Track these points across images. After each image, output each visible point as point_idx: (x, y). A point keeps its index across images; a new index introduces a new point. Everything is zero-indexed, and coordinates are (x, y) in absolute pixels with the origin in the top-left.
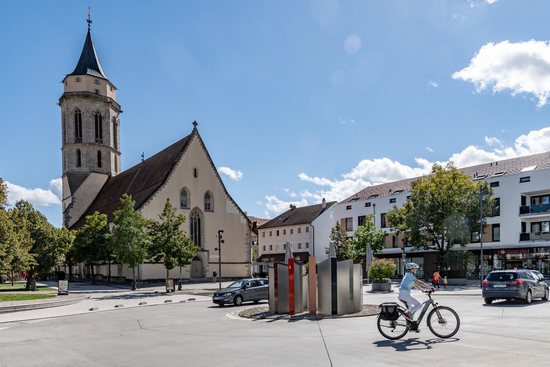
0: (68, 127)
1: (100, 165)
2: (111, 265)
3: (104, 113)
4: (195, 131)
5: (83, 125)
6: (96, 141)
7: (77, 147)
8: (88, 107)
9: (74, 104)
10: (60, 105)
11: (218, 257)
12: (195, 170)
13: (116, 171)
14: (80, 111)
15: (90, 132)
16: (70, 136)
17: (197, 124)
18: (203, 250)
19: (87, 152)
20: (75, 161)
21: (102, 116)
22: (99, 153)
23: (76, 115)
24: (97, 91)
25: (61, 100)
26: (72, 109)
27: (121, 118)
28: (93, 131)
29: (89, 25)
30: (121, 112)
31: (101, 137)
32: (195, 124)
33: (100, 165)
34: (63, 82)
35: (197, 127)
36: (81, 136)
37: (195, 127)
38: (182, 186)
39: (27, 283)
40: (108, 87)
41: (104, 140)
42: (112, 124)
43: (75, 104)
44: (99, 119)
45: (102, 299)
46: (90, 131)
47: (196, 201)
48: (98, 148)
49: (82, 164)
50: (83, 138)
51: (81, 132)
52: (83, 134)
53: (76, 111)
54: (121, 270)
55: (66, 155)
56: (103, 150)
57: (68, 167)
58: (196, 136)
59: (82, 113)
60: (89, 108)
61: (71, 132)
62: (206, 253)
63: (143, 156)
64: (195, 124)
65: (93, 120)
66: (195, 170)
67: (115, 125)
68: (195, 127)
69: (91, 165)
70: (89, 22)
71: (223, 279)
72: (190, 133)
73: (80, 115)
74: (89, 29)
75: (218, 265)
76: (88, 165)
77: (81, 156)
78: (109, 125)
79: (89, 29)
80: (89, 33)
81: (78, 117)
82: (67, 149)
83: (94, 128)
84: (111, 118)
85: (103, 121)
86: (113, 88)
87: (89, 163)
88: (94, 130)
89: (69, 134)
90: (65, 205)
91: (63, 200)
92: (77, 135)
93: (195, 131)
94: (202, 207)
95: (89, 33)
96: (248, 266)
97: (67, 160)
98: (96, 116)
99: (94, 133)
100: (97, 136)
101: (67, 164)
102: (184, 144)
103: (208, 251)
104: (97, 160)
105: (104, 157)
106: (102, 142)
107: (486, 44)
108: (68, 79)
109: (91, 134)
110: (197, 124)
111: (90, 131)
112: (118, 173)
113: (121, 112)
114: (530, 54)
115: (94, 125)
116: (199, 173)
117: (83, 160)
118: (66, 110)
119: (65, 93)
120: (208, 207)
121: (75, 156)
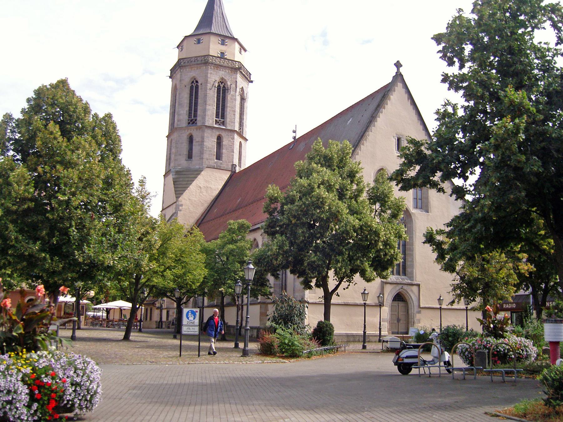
0: (179, 105)
1: (219, 156)
2: (205, 309)
4: (399, 77)
6: (217, 122)
7: (189, 132)
9: (188, 75)
10: (170, 77)
11: (201, 344)
13: (240, 166)
14: (197, 82)
16: (181, 117)
17: (401, 66)
20: (185, 152)
21: (226, 86)
22: (219, 138)
23: (192, 88)
24: (222, 53)
25: (173, 71)
26: (187, 80)
27: (251, 90)
30: (252, 82)
31: (223, 116)
32: (398, 65)
33: (219, 156)
34: (178, 47)
35: (401, 70)
36: (195, 116)
37: (398, 69)
38: (377, 168)
40: (237, 46)
41: (228, 120)
42: (238, 98)
43: (191, 74)
44: (222, 91)
49: (194, 155)
51: (196, 111)
53: (193, 82)
55: (174, 145)
56: (223, 134)
57: (175, 160)
58: (400, 85)
59: (199, 84)
61: (183, 112)
62: (415, 288)
63: (294, 132)
64: (398, 65)
67: (243, 99)
68: (398, 69)
72: (389, 80)
73: (197, 87)
78: (235, 100)
81: (195, 89)
82: (175, 136)
84: (238, 90)
86: (243, 48)
89: (179, 115)
90: (165, 216)
91: (163, 210)
93: (399, 77)
97: (173, 150)
100: (217, 116)
101: (173, 156)
102: (381, 96)
103: (418, 285)
105: (225, 145)
106: (223, 123)
107: (476, 181)
108: (185, 43)
110: (401, 66)
112: (242, 168)
113: (252, 82)
118: (178, 83)
119: (179, 60)
121: (185, 144)
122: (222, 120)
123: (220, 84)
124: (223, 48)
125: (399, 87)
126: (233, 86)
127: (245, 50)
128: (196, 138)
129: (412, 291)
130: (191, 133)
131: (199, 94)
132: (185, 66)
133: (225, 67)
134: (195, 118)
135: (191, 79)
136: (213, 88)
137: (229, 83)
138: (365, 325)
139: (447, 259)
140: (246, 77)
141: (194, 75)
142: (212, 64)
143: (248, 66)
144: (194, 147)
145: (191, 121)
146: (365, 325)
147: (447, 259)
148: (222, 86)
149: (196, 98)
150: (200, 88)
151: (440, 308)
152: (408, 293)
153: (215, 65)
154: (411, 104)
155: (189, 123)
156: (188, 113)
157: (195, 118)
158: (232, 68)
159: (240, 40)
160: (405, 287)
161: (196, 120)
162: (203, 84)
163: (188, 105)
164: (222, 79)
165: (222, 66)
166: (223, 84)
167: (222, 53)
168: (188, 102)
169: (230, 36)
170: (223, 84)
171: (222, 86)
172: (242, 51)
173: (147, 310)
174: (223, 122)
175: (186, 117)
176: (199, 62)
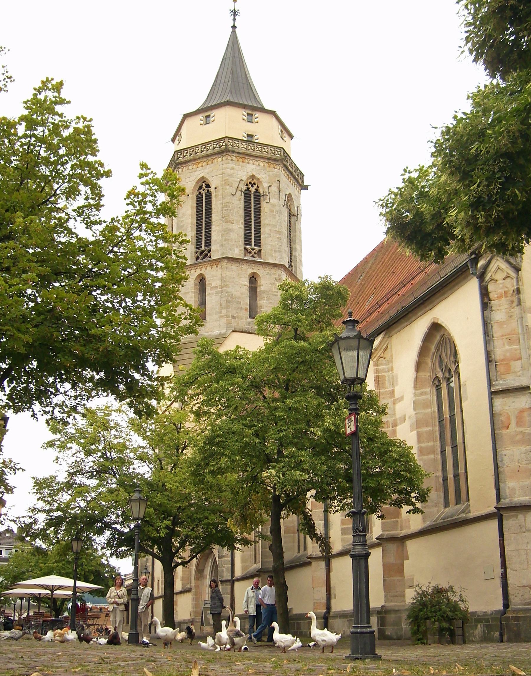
3: (266, 185)
7: (198, 272)
8: (229, 171)
14: (208, 186)
15: (231, 230)
19: (222, 279)
21: (261, 191)
22: (253, 279)
28: (238, 228)
30: (306, 188)
31: (258, 243)
36: (208, 243)
39: (219, 544)
44: (253, 199)
46: (231, 226)
48: (249, 270)
50: (213, 248)
52: (215, 236)
53: (201, 187)
54: (400, 570)
59: (212, 189)
60: (231, 175)
65: (239, 203)
67: (293, 216)
69: (233, 312)
70: (235, 13)
71: (47, 600)
73: (209, 196)
74: (234, 27)
76: (224, 312)
77: (208, 291)
79: (234, 27)
80: (234, 33)
83: (242, 220)
87: (227, 307)
88: (243, 226)
95: (234, 33)
98: (247, 195)
99: (242, 233)
100: (247, 241)
104: (247, 300)
105: (264, 292)
109: (233, 236)
111: (231, 226)
113: (306, 188)
114: (331, 545)
115: (242, 212)
122: (258, 248)
123: (250, 186)
126: (274, 189)
127: (291, 137)
130: (201, 275)
131: (213, 206)
132: (186, 162)
133: (257, 157)
134: (208, 248)
135: (197, 182)
136: (239, 193)
137: (266, 185)
139: (114, 562)
140: (295, 178)
141: (201, 175)
142: (233, 152)
143: (298, 157)
145: (201, 253)
147: (114, 562)
148: (253, 190)
149: (209, 225)
150: (213, 195)
153: (238, 153)
155: (198, 258)
157: (208, 248)
158: (269, 159)
159: (279, 114)
161: (209, 251)
162: (220, 188)
163: (195, 228)
164: (253, 177)
165: (251, 156)
166: (255, 187)
168: (195, 221)
169: (259, 106)
170: (255, 187)
171: (253, 190)
172: (286, 135)
173: (305, 548)
174: (260, 251)
176: (210, 152)
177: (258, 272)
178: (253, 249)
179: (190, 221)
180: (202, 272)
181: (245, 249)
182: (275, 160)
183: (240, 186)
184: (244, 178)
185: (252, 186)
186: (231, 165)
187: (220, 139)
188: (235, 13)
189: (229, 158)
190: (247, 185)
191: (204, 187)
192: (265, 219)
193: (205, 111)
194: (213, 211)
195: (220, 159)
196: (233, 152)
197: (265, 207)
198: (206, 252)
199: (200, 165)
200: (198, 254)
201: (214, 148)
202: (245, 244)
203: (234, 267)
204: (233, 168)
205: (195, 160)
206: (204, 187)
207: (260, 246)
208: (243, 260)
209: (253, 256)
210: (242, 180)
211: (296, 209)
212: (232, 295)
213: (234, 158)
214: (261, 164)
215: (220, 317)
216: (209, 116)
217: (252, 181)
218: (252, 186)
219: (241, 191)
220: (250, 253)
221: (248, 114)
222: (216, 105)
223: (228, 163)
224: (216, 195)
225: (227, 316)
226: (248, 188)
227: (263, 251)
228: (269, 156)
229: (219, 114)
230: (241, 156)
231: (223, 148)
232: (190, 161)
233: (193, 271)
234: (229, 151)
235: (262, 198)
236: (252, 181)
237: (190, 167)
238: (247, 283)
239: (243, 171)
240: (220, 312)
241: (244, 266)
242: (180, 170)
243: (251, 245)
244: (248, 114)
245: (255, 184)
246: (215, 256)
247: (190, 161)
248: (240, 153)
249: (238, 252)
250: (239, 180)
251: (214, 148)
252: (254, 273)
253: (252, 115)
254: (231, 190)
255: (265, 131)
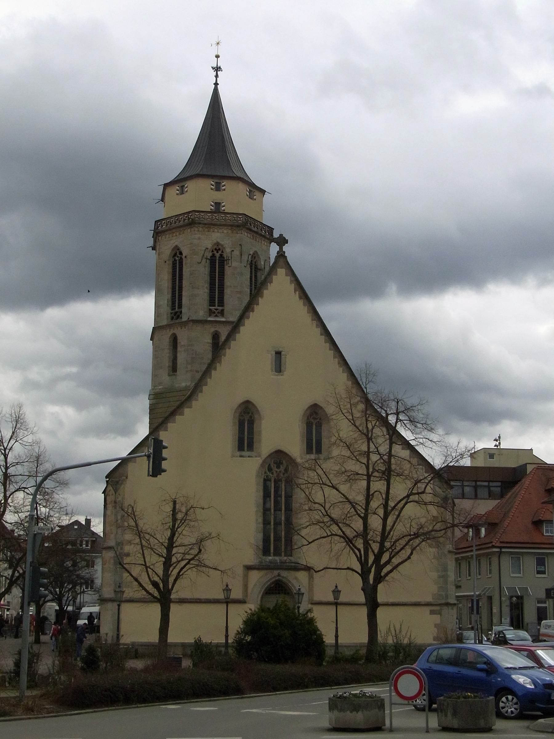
5: (185, 283)
6: (211, 313)
7: (172, 331)
9: (168, 244)
10: (154, 248)
12: (278, 354)
14: (181, 253)
17: (286, 242)
18: (296, 568)
21: (225, 255)
28: (203, 292)
29: (217, 76)
31: (221, 303)
35: (285, 248)
36: (180, 306)
38: (240, 399)
43: (172, 242)
45: (290, 693)
47: (281, 432)
49: (178, 367)
52: (185, 301)
53: (175, 255)
59: (183, 257)
62: (302, 576)
65: (203, 270)
66: (278, 354)
70: (217, 69)
74: (216, 84)
75: (125, 607)
77: (179, 349)
79: (216, 84)
83: (207, 285)
85: (226, 267)
88: (207, 291)
92: (173, 308)
94: (295, 448)
96: (440, 613)
98: (212, 260)
100: (212, 302)
106: (222, 313)
110: (286, 242)
116: (288, 361)
117: (181, 357)
120: (314, 444)
121: (167, 351)
122: (220, 308)
123: (215, 252)
124: (218, 196)
125: (281, 272)
126: (237, 253)
127: (263, 192)
128: (182, 341)
129: (296, 578)
133: (220, 225)
134: (180, 310)
135: (173, 250)
136: (204, 260)
137: (228, 250)
138: (337, 628)
141: (176, 244)
142: (200, 223)
144: (178, 355)
146: (337, 628)
148: (218, 255)
151: (227, 603)
152: (290, 582)
154: (300, 298)
155: (172, 318)
156: (170, 303)
157: (180, 310)
160: (284, 574)
163: (170, 290)
164: (218, 244)
166: (220, 252)
167: (218, 205)
171: (218, 255)
174: (223, 310)
175: (206, 303)
177: (219, 330)
178: (216, 309)
179: (166, 285)
180: (174, 332)
181: (210, 310)
182: (238, 226)
183: (205, 255)
184: (209, 246)
185: (217, 252)
186: (197, 236)
187: (189, 212)
188: (217, 69)
189: (196, 229)
190: (213, 251)
191: (178, 253)
192: (228, 282)
193: (180, 182)
194: (184, 277)
195: (189, 230)
196: (200, 223)
197: (228, 271)
198: (178, 314)
199: (174, 235)
200: (173, 315)
201: (184, 220)
202: (210, 306)
203: (199, 328)
204: (199, 239)
205: (170, 230)
206: (178, 253)
207: (223, 306)
208: (206, 322)
209: (216, 316)
210: (207, 249)
211: (262, 263)
212: (196, 352)
213: (201, 229)
214: (225, 231)
215: (187, 371)
216: (184, 186)
217: (218, 248)
218: (217, 252)
219: (207, 259)
220: (214, 313)
221: (216, 183)
222: (188, 177)
223: (196, 234)
224: (186, 263)
225: (191, 371)
226: (213, 254)
227: (225, 311)
228: (232, 223)
229: (191, 185)
230: (207, 226)
231: (190, 221)
232: (167, 231)
233: (168, 330)
234: (195, 223)
235: (225, 262)
236: (218, 248)
237: (167, 236)
238: (210, 341)
239: (206, 240)
240: (187, 367)
241: (207, 326)
242: (160, 238)
243: (214, 306)
244: (216, 183)
245: (219, 249)
246: (185, 318)
247: (167, 231)
248: (206, 224)
249: (201, 314)
250: (204, 248)
251: (184, 220)
252: (216, 331)
253: (220, 183)
254: (198, 258)
255: (233, 198)
